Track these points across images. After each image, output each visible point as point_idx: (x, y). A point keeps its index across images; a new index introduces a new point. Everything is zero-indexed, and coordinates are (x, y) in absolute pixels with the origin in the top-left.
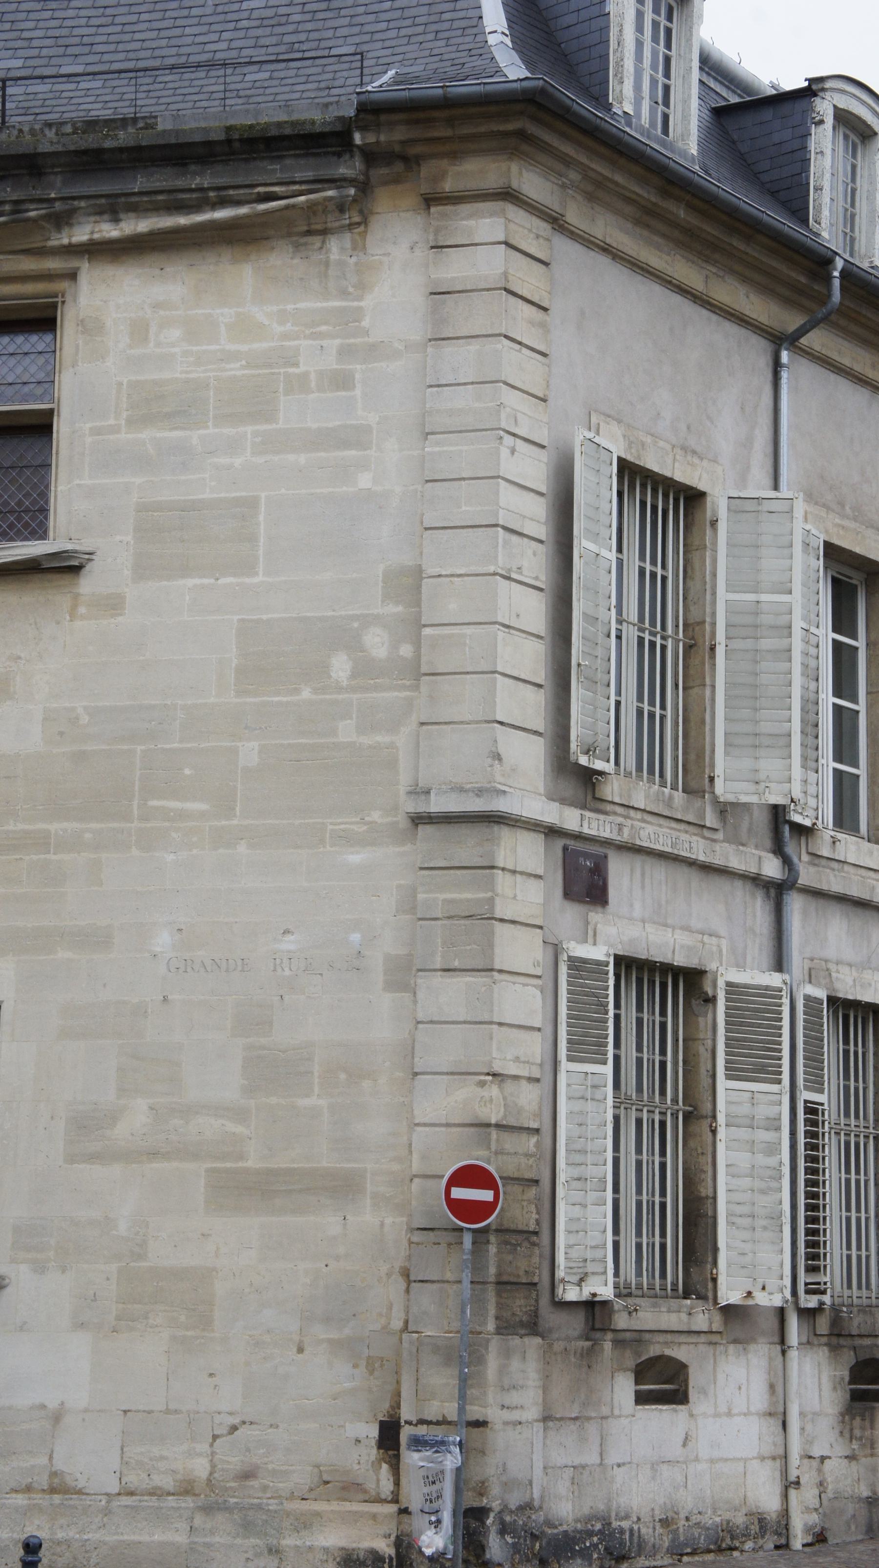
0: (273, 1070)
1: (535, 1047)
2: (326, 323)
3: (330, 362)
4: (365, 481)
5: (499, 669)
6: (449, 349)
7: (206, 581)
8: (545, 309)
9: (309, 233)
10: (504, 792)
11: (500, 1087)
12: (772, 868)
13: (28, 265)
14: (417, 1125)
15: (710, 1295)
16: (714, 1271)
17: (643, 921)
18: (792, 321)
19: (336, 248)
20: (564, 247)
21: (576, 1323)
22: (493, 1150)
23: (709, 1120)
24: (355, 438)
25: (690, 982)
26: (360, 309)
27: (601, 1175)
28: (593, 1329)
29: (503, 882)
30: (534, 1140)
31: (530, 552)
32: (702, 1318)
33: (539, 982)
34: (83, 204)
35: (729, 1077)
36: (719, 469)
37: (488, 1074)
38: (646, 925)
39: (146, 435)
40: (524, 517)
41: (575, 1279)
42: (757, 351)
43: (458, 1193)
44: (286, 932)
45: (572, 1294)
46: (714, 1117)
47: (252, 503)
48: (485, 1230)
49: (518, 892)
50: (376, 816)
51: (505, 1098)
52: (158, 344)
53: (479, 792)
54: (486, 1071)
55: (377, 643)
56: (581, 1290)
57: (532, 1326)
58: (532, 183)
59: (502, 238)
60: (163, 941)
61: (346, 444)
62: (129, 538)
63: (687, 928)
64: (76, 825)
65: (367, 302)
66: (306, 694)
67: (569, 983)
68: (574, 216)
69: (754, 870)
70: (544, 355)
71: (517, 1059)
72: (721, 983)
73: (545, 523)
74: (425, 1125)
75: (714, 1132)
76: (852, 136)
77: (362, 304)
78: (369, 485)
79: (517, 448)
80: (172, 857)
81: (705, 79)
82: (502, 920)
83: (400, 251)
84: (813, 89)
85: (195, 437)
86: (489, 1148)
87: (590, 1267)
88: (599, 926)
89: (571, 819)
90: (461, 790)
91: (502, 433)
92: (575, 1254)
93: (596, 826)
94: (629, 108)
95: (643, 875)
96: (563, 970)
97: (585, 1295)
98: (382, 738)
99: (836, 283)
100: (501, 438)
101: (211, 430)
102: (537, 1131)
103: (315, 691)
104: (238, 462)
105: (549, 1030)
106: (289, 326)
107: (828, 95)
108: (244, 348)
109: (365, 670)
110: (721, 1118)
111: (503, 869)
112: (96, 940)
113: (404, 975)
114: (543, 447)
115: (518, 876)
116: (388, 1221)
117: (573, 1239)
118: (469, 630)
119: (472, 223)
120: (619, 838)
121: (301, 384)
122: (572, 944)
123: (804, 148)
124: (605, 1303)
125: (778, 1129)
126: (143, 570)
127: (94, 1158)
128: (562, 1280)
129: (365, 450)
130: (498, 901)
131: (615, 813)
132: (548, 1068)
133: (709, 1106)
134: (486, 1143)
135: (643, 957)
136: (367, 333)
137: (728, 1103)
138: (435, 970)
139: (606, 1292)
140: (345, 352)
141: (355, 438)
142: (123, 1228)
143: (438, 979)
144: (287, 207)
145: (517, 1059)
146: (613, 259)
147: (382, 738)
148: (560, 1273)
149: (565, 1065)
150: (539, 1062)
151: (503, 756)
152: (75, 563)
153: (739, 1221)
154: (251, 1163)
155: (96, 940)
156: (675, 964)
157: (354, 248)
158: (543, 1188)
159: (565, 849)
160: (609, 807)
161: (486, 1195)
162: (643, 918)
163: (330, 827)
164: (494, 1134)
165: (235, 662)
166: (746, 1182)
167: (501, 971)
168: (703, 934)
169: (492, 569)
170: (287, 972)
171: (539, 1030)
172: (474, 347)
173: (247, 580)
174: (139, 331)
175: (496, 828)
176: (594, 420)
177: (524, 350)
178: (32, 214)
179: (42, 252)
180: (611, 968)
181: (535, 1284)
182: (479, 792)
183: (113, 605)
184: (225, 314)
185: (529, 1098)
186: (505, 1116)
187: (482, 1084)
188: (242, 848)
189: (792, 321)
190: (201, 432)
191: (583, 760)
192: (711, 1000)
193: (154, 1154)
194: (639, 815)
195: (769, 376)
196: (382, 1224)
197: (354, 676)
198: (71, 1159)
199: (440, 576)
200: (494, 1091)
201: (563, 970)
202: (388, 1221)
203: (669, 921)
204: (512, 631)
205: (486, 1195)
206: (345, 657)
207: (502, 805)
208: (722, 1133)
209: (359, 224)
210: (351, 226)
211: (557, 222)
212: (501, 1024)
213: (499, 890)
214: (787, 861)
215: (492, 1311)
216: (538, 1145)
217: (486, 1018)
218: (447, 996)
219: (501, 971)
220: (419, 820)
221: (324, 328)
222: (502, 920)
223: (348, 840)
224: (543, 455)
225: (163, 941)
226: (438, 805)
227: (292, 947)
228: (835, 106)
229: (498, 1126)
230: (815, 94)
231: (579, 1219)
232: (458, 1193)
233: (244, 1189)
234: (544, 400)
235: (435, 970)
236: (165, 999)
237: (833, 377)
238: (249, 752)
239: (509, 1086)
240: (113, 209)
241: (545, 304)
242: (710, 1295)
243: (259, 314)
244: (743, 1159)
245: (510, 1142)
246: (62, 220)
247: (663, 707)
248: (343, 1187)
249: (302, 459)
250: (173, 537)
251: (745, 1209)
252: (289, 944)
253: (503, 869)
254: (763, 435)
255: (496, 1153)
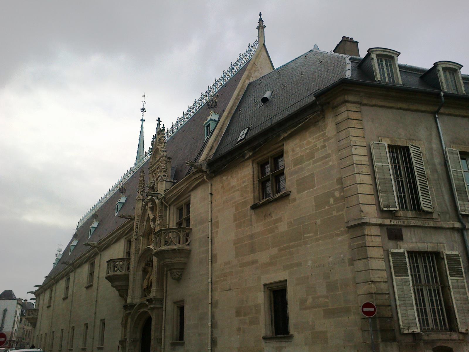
0: (331, 287)
1: (385, 274)
2: (320, 137)
3: (322, 144)
4: (331, 163)
5: (359, 193)
6: (340, 133)
7: (308, 191)
8: (361, 120)
9: (316, 122)
10: (364, 218)
11: (374, 284)
12: (457, 225)
13: (277, 146)
14: (359, 295)
15: (457, 330)
16: (457, 324)
17: (416, 242)
18: (436, 108)
19: (320, 124)
20: (364, 108)
21: (410, 339)
22: (374, 299)
23: (448, 287)
24: (328, 156)
25: (437, 255)
26: (326, 132)
27: (412, 302)
28: (416, 340)
29: (367, 238)
30: (387, 296)
31: (365, 168)
32: (455, 336)
33: (383, 259)
34: (281, 132)
35: (451, 276)
36: (422, 142)
37: (370, 282)
38: (417, 243)
39: (296, 167)
40: (362, 161)
41: (406, 328)
42: (430, 118)
43: (365, 309)
44: (330, 257)
45: (406, 332)
46: (449, 287)
47: (313, 174)
48: (375, 318)
49: (373, 240)
50: (342, 229)
51: (376, 287)
52: (296, 151)
53: (358, 219)
54: (370, 281)
55: (337, 194)
56: (409, 330)
57: (394, 340)
58: (351, 98)
59: (346, 110)
60: (310, 262)
61: (327, 158)
62: (296, 187)
63: (431, 243)
64: (294, 243)
65: (327, 131)
66: (327, 208)
67: (392, 259)
68: (365, 101)
69: (451, 226)
70: (363, 129)
71: (379, 277)
72: (444, 254)
73: (368, 161)
74: (360, 295)
75: (450, 290)
76: (451, 72)
77: (326, 131)
78: (331, 164)
79: (357, 148)
80: (309, 246)
81: (400, 70)
82: (369, 247)
83: (330, 120)
84: (436, 64)
85: (303, 165)
86: (373, 299)
87: (411, 325)
88: (401, 245)
89: (387, 222)
90: (355, 220)
91: (352, 146)
92: (406, 322)
93: (394, 222)
94: (379, 79)
95: (414, 232)
96: (390, 256)
97: (411, 331)
98: (341, 213)
99: (443, 98)
100: (352, 147)
101: (306, 163)
102: (388, 294)
103: (328, 207)
104: (310, 167)
105: (388, 270)
106: (315, 140)
107: (439, 65)
108: (308, 147)
109: (336, 200)
110: (451, 287)
111: (367, 235)
112: (299, 265)
113: (352, 262)
114: (365, 146)
115: (372, 236)
116: (357, 317)
117: (404, 318)
118: (352, 186)
119: (340, 109)
120: (404, 224)
121: (318, 149)
122: (392, 250)
123: (437, 77)
124: (418, 333)
125: (465, 289)
126: (299, 192)
127: (305, 309)
128: (402, 328)
129: (330, 157)
130: (366, 242)
131: (403, 219)
132: (390, 279)
133: (447, 284)
134: (372, 297)
135: (417, 251)
136: (327, 136)
137: (452, 283)
138: (357, 260)
139: (418, 330)
140: (325, 141)
141: (328, 156)
142: (310, 324)
143: (357, 262)
144: (310, 119)
145: (379, 277)
146: (372, 107)
147: (341, 213)
148: (402, 326)
149: (394, 278)
150: (386, 277)
151: (363, 210)
152: (288, 194)
153: (460, 311)
154: (330, 307)
155: (299, 265)
156: (429, 251)
157: (323, 122)
158: (391, 306)
159: (387, 229)
160: (400, 218)
161: (373, 309)
162: (412, 241)
163: (334, 233)
164: (374, 295)
165: (314, 205)
166: (460, 302)
167: (370, 258)
168: (438, 243)
169: (354, 173)
170: (331, 265)
171: (385, 270)
172: (345, 131)
173: (314, 189)
174: (293, 150)
175: (364, 226)
176: (380, 138)
177: (356, 129)
178: (274, 137)
179: (278, 143)
180: (406, 254)
181: (394, 330)
182: (358, 219)
183: (295, 200)
184: (305, 142)
185: (384, 287)
186: (377, 290)
187: (369, 284)
188: (320, 241)
189: (436, 108)
190: (304, 164)
191: (385, 209)
192: (443, 259)
193: (314, 307)
194: (411, 219)
195: (434, 120)
196: (356, 318)
197: (334, 202)
198: (301, 309)
199: (345, 177)
200: (373, 285)
201: (390, 256)
202: (357, 317)
203: (425, 242)
204: (362, 184)
205: (373, 309)
206: (332, 198)
207: (363, 221)
208: (452, 290)
209: (323, 118)
210: (322, 118)
211: (361, 104)
212: (372, 270)
213: (367, 239)
214: (462, 224)
215: (380, 337)
216: (389, 297)
217: (368, 269)
218: (360, 265)
219: (370, 258)
220: (349, 227)
221: (320, 138)
222: (369, 247)
223: (338, 235)
224: (365, 148)
225: (310, 262)
226: (351, 224)
227: (331, 260)
228: (442, 67)
229: (375, 293)
230: (436, 66)
231: (405, 313)
232: (365, 309)
233: (330, 313)
234: (364, 137)
235: (357, 260)
236: (312, 275)
237: (455, 118)
238: (319, 221)
239: (377, 284)
240: (285, 131)
241: (361, 119)
242: (457, 330)
243: (310, 140)
244: (458, 296)
245: (379, 297)
246: (279, 136)
247: (404, 193)
248: (347, 311)
249: (320, 163)
250: (304, 184)
251: (461, 308)
252: (331, 259)
253: (367, 235)
254: (434, 133)
255: (375, 300)
